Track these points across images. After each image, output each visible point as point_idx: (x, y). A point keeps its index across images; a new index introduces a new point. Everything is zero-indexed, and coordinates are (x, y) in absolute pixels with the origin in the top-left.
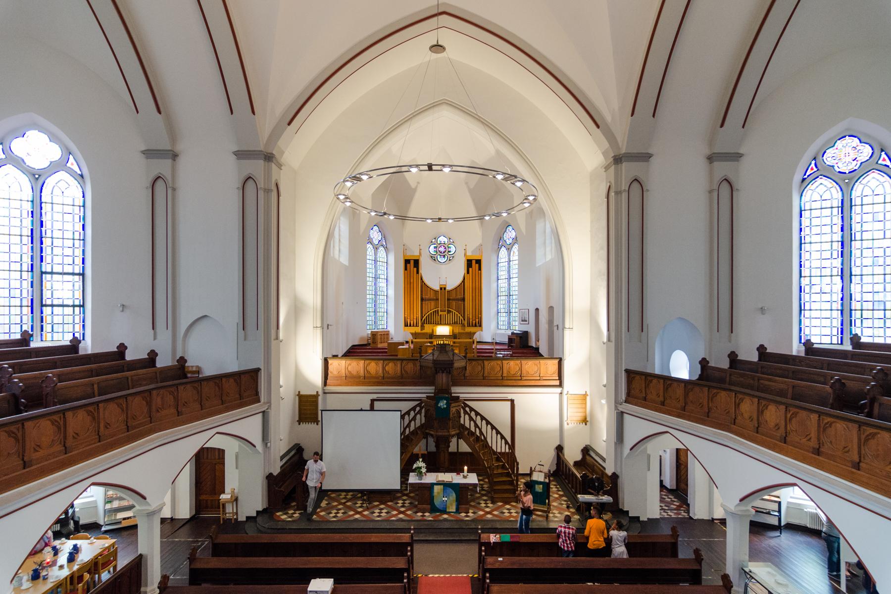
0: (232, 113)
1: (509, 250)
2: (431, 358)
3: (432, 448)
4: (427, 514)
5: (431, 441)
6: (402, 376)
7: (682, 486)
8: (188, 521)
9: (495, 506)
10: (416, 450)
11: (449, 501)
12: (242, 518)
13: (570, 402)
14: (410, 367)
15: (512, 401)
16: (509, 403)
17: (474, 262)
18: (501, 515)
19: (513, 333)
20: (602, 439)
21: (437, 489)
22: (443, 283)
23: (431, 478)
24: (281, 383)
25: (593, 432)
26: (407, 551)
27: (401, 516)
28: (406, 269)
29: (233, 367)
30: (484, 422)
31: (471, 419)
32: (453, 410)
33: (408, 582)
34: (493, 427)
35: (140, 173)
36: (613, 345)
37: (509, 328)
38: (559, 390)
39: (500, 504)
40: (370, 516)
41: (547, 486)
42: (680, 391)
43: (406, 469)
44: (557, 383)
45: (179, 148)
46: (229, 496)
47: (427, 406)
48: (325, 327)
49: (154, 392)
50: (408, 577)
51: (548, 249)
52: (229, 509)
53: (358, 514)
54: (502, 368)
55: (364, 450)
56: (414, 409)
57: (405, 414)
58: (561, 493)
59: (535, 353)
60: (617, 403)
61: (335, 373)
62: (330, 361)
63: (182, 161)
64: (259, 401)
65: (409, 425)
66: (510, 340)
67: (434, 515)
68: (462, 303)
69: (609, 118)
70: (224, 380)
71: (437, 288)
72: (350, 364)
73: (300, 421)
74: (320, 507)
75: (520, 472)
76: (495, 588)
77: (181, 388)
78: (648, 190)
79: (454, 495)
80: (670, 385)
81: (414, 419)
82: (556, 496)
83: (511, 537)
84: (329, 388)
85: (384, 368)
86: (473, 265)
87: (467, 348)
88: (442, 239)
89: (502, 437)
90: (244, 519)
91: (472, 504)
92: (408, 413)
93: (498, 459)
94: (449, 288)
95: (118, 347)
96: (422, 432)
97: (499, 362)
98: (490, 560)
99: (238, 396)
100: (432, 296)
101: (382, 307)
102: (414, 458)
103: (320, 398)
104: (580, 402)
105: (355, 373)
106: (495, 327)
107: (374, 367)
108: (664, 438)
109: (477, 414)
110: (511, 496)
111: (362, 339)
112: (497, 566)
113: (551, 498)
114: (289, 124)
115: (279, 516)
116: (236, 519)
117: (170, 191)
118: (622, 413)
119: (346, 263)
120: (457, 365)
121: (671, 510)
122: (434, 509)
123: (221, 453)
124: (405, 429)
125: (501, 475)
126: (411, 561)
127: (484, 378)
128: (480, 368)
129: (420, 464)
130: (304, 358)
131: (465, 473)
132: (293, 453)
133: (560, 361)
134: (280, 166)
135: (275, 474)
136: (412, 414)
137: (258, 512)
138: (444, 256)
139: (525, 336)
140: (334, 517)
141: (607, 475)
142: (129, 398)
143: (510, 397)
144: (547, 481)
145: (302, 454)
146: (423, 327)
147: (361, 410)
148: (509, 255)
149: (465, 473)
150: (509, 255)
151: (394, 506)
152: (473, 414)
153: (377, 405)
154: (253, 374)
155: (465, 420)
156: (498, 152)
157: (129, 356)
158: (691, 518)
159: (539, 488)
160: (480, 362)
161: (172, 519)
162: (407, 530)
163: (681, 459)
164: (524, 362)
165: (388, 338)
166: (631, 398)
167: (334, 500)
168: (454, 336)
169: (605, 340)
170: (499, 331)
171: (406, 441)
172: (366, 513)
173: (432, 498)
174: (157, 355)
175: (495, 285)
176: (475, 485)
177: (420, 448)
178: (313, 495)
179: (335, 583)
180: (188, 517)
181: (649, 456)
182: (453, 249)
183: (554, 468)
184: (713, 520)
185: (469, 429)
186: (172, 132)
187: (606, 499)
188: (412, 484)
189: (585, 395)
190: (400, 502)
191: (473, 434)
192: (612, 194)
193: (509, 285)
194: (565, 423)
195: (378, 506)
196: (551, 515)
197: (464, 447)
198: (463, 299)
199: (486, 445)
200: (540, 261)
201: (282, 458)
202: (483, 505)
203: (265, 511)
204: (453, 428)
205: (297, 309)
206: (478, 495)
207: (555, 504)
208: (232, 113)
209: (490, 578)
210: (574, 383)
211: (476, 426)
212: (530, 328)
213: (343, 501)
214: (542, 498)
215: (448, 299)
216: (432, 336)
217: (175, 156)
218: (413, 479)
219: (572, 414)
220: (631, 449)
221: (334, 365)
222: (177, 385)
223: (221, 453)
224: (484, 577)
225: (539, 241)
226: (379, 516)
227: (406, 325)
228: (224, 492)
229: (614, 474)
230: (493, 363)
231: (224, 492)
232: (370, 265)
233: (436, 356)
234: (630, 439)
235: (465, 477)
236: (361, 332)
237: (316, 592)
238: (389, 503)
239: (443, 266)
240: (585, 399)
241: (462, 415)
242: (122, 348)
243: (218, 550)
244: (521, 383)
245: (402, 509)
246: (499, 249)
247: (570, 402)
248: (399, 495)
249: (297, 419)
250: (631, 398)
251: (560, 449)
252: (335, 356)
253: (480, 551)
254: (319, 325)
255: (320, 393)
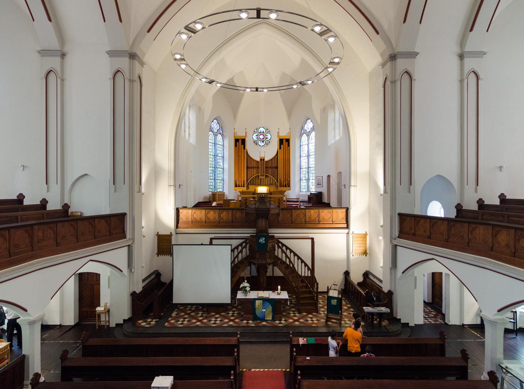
0: (105, 21)
1: (308, 136)
2: (253, 206)
3: (255, 273)
4: (250, 322)
5: (253, 267)
6: (233, 221)
7: (437, 300)
8: (71, 328)
9: (301, 315)
10: (242, 275)
11: (267, 312)
12: (113, 325)
13: (354, 239)
14: (238, 214)
15: (312, 239)
16: (310, 240)
17: (284, 141)
18: (306, 322)
19: (311, 194)
20: (379, 266)
21: (258, 303)
22: (262, 156)
23: (253, 295)
24: (143, 225)
25: (371, 260)
26: (234, 352)
27: (231, 323)
28: (236, 146)
29: (106, 211)
30: (292, 254)
31: (283, 251)
32: (270, 245)
33: (235, 378)
34: (299, 258)
35: (38, 67)
36: (388, 196)
37: (308, 190)
38: (346, 231)
39: (305, 314)
40: (208, 323)
41: (339, 300)
42: (444, 227)
43: (235, 288)
44: (345, 226)
45: (66, 49)
46: (103, 309)
47: (250, 242)
48: (177, 186)
49: (36, 227)
50: (235, 374)
51: (337, 131)
52: (103, 318)
53: (199, 322)
54: (305, 215)
55: (206, 275)
56: (241, 245)
57: (234, 249)
58: (349, 306)
59: (328, 206)
60: (392, 238)
61: (184, 219)
62: (181, 211)
63: (68, 58)
64: (125, 237)
65: (237, 256)
66: (309, 197)
67: (255, 322)
68: (277, 170)
69: (385, 26)
70: (96, 220)
71: (259, 160)
72: (195, 213)
73: (159, 254)
74: (171, 316)
75: (319, 291)
76: (306, 383)
77: (60, 225)
78: (415, 80)
79: (271, 307)
80: (435, 223)
81: (241, 251)
82: (346, 308)
83: (315, 339)
84: (180, 230)
85: (219, 216)
86: (284, 143)
87: (280, 200)
88: (262, 130)
89: (306, 265)
90: (114, 326)
91: (284, 314)
92: (237, 248)
93: (302, 281)
94: (266, 159)
95: (17, 197)
96: (248, 261)
97: (303, 211)
98: (300, 358)
99: (108, 233)
100: (255, 165)
101: (220, 176)
102: (242, 280)
103: (173, 237)
104: (361, 239)
105: (198, 219)
106: (301, 187)
107: (212, 215)
108: (424, 263)
109: (287, 248)
110: (314, 309)
111: (205, 198)
112: (305, 364)
113: (343, 310)
114: (149, 31)
115: (140, 324)
116: (108, 326)
117: (59, 80)
118: (396, 245)
119: (194, 143)
120: (272, 212)
121: (431, 318)
122: (255, 318)
123: (98, 276)
124: (234, 259)
125: (305, 292)
126: (237, 360)
127: (292, 222)
128: (289, 215)
129: (246, 284)
130: (161, 208)
131: (279, 291)
132: (153, 276)
133: (347, 210)
134: (142, 64)
135: (138, 292)
136: (240, 248)
137: (124, 320)
138: (263, 142)
139: (319, 195)
140: (181, 324)
141: (383, 292)
142: (11, 230)
143: (311, 236)
144: (340, 296)
145: (160, 278)
146: (248, 188)
147: (202, 244)
148: (308, 140)
149: (279, 291)
150: (308, 140)
151: (226, 315)
152: (284, 248)
153: (214, 242)
154: (121, 217)
155: (278, 253)
156: (303, 61)
157: (26, 202)
158: (446, 324)
159: (334, 302)
160: (290, 211)
161: (60, 325)
162: (234, 334)
163: (436, 281)
164: (321, 211)
165: (223, 197)
166: (402, 234)
167: (182, 311)
168: (270, 193)
169: (382, 192)
170: (301, 193)
171: (235, 269)
172: (205, 321)
173: (254, 309)
174: (47, 202)
175: (299, 160)
176: (286, 300)
177: (246, 273)
178: (514, 310)
179: (175, 379)
180: (72, 323)
181: (416, 278)
182: (269, 137)
183: (343, 287)
184: (463, 325)
185: (281, 260)
186: (62, 38)
187: (384, 309)
188: (239, 300)
189: (366, 235)
190: (231, 312)
191: (284, 263)
192: (388, 83)
193: (308, 160)
194: (351, 255)
195: (214, 315)
196: (343, 322)
197: (278, 273)
198: (277, 168)
199: (293, 271)
200: (331, 141)
201: (144, 281)
202: (292, 315)
203: (129, 319)
204: (270, 258)
205: (156, 172)
206: (288, 307)
207: (345, 314)
208: (105, 21)
209: (301, 375)
210: (357, 226)
211: (287, 256)
212: (324, 190)
213: (189, 312)
214: (334, 309)
215: (266, 168)
216: (254, 193)
217: (63, 55)
218: (240, 295)
219: (356, 248)
220: (403, 273)
221: (183, 213)
222: (56, 222)
223: (98, 276)
224: (296, 374)
225: (330, 126)
226: (214, 323)
227: (236, 186)
228: (99, 305)
229: (389, 291)
230: (298, 211)
231: (99, 305)
232: (211, 147)
233: (257, 205)
234: (402, 265)
235: (278, 294)
236: (205, 193)
237: (158, 387)
238: (223, 314)
239: (263, 148)
240: (366, 237)
241: (276, 248)
242: (21, 198)
243: (87, 351)
244: (319, 226)
245: (232, 318)
246: (301, 135)
247: (354, 239)
248: (230, 307)
249: (156, 252)
250: (402, 234)
251: (347, 274)
252: (185, 207)
253: (292, 352)
254: (172, 184)
255: (173, 233)
